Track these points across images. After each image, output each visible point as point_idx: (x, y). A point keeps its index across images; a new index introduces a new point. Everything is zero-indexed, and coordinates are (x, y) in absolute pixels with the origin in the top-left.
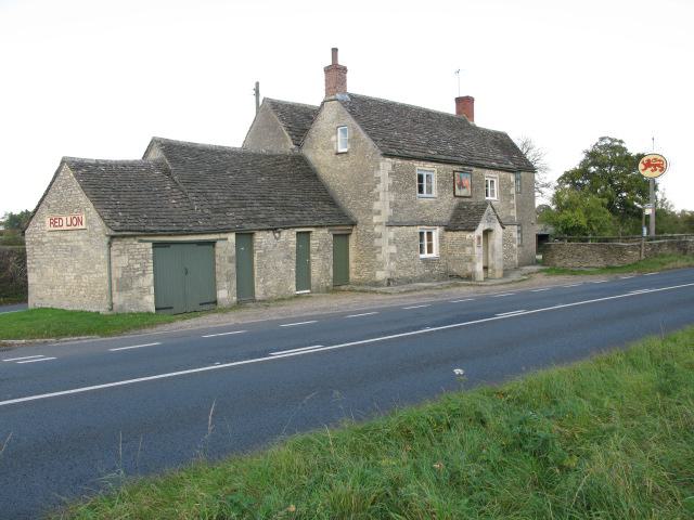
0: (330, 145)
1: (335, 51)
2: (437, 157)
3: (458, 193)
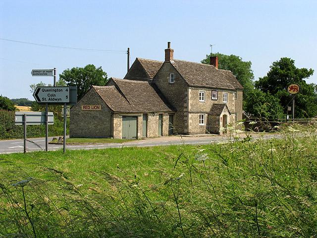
0: (167, 80)
1: (169, 43)
2: (206, 86)
3: (213, 98)
